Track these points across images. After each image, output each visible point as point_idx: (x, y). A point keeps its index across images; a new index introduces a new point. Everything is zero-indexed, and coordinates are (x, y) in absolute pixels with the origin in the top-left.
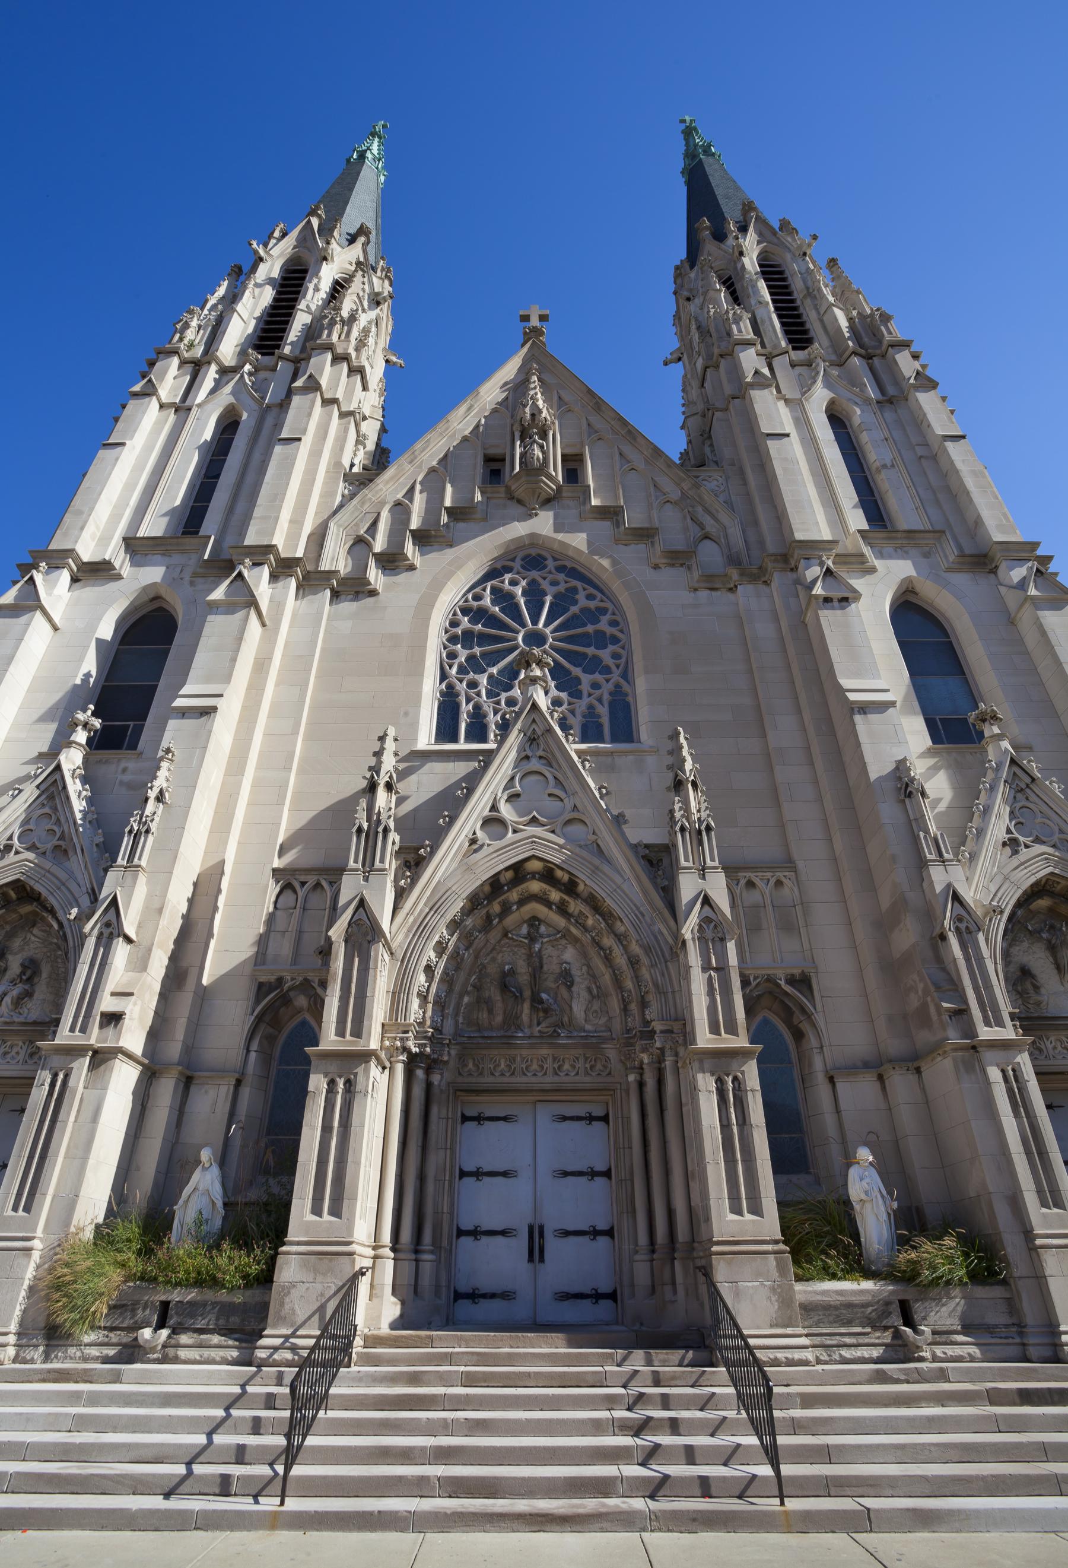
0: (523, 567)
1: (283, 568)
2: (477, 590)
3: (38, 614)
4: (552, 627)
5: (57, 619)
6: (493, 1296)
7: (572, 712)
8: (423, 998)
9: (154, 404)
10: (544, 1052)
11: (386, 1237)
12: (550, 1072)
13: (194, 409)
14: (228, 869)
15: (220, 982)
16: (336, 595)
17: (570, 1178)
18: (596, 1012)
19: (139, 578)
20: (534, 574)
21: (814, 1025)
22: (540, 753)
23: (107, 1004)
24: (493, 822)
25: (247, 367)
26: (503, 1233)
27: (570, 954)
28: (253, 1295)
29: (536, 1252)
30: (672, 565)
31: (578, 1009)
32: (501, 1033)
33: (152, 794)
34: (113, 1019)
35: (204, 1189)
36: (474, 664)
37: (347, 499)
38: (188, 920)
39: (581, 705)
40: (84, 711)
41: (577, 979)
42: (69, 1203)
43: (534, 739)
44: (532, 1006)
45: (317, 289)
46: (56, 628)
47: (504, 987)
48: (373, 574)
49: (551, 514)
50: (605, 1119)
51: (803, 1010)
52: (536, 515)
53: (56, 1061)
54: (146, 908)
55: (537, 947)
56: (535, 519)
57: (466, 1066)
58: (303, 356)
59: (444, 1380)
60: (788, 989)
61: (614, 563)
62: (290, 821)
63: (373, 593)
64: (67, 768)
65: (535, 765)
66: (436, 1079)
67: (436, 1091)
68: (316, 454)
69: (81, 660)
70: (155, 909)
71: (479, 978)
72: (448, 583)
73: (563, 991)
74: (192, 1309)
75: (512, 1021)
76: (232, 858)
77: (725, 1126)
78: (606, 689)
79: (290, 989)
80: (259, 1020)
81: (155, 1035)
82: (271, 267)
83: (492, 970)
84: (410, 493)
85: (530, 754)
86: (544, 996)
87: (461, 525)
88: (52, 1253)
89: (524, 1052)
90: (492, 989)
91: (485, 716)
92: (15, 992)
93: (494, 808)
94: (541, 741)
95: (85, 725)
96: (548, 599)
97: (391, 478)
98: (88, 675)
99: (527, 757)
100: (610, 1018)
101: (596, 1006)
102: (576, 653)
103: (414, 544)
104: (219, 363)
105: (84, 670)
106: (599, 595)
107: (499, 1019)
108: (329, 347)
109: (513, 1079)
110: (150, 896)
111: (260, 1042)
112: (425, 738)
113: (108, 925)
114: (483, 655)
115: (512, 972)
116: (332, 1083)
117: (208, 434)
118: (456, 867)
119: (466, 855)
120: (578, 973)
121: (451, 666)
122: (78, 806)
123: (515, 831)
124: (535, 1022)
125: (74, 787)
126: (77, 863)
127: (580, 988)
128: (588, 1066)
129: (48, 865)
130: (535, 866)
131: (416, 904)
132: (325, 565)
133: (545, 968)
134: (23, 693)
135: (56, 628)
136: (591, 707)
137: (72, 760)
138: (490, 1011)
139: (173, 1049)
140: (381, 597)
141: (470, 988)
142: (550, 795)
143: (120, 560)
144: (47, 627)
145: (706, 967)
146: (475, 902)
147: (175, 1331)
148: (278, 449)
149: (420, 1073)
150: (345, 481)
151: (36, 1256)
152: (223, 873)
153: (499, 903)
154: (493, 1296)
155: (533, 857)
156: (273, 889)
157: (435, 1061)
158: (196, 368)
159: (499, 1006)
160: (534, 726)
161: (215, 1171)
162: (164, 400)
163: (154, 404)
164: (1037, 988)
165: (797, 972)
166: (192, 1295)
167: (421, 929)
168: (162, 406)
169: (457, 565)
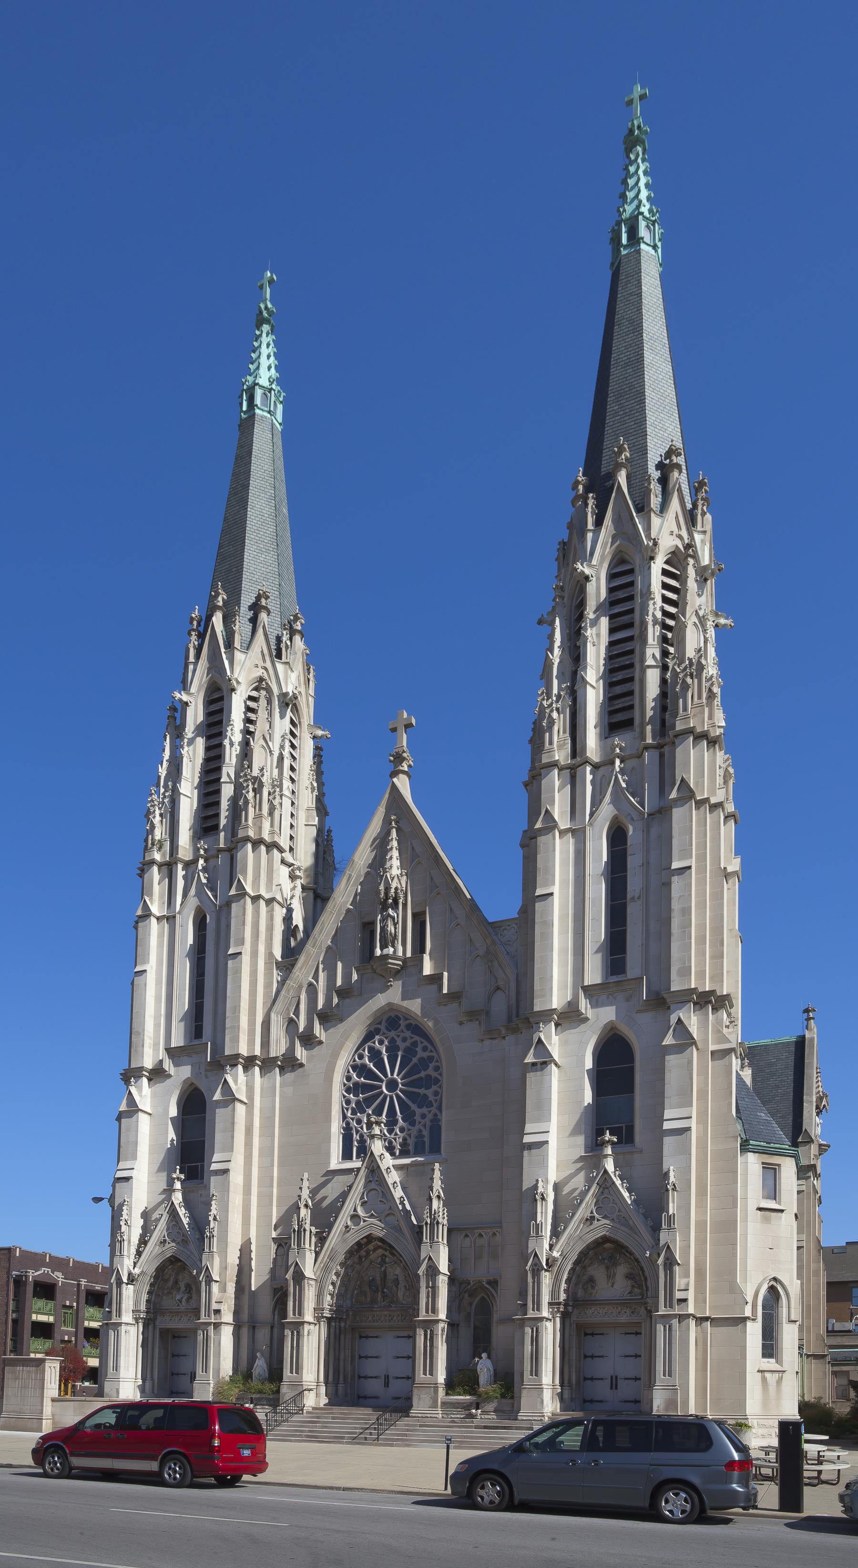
0: (387, 1029)
1: (249, 1062)
2: (360, 1051)
3: (140, 1114)
4: (401, 1075)
5: (149, 1111)
7: (410, 1135)
8: (332, 1295)
9: (154, 921)
10: (386, 1313)
11: (322, 1378)
13: (177, 916)
14: (253, 1241)
15: (259, 1289)
16: (282, 1069)
19: (180, 1074)
20: (393, 1034)
22: (376, 1179)
23: (214, 1306)
24: (355, 1217)
25: (201, 862)
26: (375, 1377)
27: (398, 1271)
28: (275, 1396)
30: (471, 1020)
31: (400, 1295)
33: (211, 1218)
34: (217, 1312)
35: (260, 1366)
36: (360, 1108)
37: (282, 983)
38: (240, 1267)
39: (414, 1131)
40: (175, 1172)
42: (217, 1370)
45: (232, 744)
46: (150, 1114)
48: (300, 1053)
49: (400, 982)
52: (391, 985)
53: (203, 1327)
54: (221, 1267)
56: (391, 989)
58: (233, 846)
59: (326, 1418)
61: (436, 1022)
62: (278, 1212)
63: (301, 1065)
64: (176, 1203)
65: (373, 1185)
68: (254, 954)
69: (167, 1133)
70: (224, 1268)
72: (340, 1052)
73: (394, 1287)
74: (259, 1399)
75: (374, 1301)
76: (255, 1234)
77: (425, 1347)
78: (430, 1116)
81: (236, 1313)
82: (195, 715)
84: (316, 977)
87: (347, 1001)
88: (215, 1385)
91: (366, 1141)
92: (185, 1298)
93: (355, 1210)
95: (178, 1179)
96: (400, 1054)
97: (303, 965)
98: (172, 1140)
99: (370, 1181)
102: (414, 1093)
103: (320, 1024)
104: (182, 861)
105: (170, 1139)
106: (430, 1047)
107: (369, 1299)
108: (247, 839)
110: (221, 1262)
112: (335, 1162)
113: (207, 1277)
114: (365, 1099)
115: (374, 1280)
116: (292, 1332)
117: (190, 940)
118: (339, 1239)
119: (344, 1234)
120: (401, 1279)
121: (347, 1109)
122: (185, 1221)
123: (364, 1221)
125: (182, 1212)
126: (192, 1246)
127: (401, 1286)
129: (182, 1248)
131: (323, 1258)
132: (273, 1054)
134: (147, 1156)
135: (150, 1114)
136: (420, 1131)
137: (178, 1198)
138: (366, 1297)
139: (245, 1317)
140: (306, 1067)
143: (168, 1065)
144: (146, 1116)
145: (427, 1287)
146: (350, 1253)
147: (256, 1405)
148: (230, 963)
149: (333, 1324)
150: (277, 968)
151: (212, 1385)
152: (251, 1243)
156: (274, 1247)
158: (168, 868)
161: (263, 1359)
162: (158, 914)
163: (154, 921)
164: (593, 1287)
165: (491, 1278)
166: (258, 1396)
167: (326, 1269)
168: (158, 919)
169: (346, 1036)
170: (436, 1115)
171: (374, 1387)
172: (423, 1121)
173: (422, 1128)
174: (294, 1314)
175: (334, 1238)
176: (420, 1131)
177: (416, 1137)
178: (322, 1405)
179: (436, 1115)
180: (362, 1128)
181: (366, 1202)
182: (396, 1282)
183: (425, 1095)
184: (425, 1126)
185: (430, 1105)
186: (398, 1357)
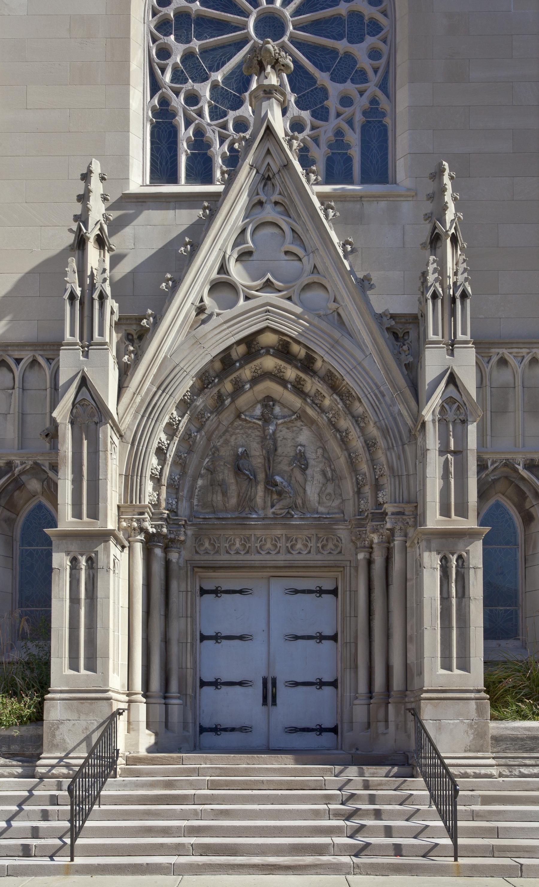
6: (233, 730)
8: (157, 480)
10: (278, 532)
12: (283, 550)
17: (300, 642)
18: (329, 494)
22: (276, 197)
24: (222, 286)
26: (241, 684)
27: (305, 436)
28: (29, 730)
29: (269, 695)
31: (312, 492)
32: (236, 515)
36: (193, 68)
41: (312, 462)
43: (269, 178)
44: (265, 487)
47: (238, 470)
50: (334, 592)
55: (271, 428)
57: (202, 545)
60: (525, 474)
66: (174, 556)
67: (174, 567)
71: (213, 461)
73: (297, 473)
75: (246, 503)
78: (361, 103)
79: (23, 472)
83: (225, 452)
85: (264, 198)
86: (278, 479)
89: (258, 533)
90: (226, 472)
93: (223, 269)
94: (277, 181)
99: (260, 203)
100: (343, 501)
101: (330, 489)
107: (233, 501)
109: (248, 557)
112: (138, 178)
114: (204, 51)
115: (246, 455)
116: (74, 561)
119: (194, 326)
127: (315, 470)
128: (320, 545)
130: (269, 339)
131: (142, 382)
133: (280, 450)
136: (339, 133)
138: (225, 494)
145: (444, 451)
149: (158, 552)
153: (231, 381)
154: (233, 730)
155: (267, 329)
157: (172, 541)
159: (233, 489)
160: (269, 160)
167: (149, 410)
170: (374, 101)
171: (239, 706)
172: (348, 111)
173: (345, 127)
174: (77, 514)
175: (170, 335)
176: (339, 133)
177: (330, 147)
178: (142, 752)
179: (374, 101)
180: (200, 114)
181: (249, 253)
183: (348, 56)
184: (350, 122)
185: (361, 77)
186: (296, 638)
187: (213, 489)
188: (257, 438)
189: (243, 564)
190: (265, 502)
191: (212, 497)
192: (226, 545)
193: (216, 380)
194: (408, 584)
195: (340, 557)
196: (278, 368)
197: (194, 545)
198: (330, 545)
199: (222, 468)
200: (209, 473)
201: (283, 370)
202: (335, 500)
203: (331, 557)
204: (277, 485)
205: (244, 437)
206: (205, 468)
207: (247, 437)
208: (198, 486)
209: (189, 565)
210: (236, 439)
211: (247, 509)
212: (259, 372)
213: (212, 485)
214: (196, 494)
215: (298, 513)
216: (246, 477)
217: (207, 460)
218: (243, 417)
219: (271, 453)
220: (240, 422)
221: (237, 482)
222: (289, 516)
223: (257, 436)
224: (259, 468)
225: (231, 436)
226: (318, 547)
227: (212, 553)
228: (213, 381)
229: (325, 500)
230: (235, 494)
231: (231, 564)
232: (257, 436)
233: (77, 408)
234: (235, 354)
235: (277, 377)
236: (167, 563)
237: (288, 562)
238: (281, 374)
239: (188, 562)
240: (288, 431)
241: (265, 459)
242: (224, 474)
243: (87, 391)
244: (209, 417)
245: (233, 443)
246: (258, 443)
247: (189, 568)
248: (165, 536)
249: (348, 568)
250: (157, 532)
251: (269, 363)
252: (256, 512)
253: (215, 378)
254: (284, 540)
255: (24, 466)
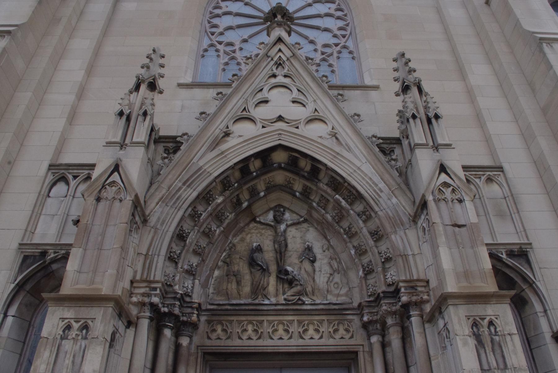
12: (296, 335)
18: (337, 283)
21: (536, 292)
31: (321, 280)
32: (249, 301)
41: (319, 256)
43: (280, 64)
44: (277, 277)
47: (252, 263)
51: (525, 279)
55: (283, 227)
57: (214, 330)
66: (184, 341)
67: (184, 352)
71: (229, 256)
73: (307, 265)
75: (258, 290)
80: (20, 287)
86: (289, 269)
89: (271, 318)
90: (241, 264)
101: (337, 278)
107: (247, 289)
109: (260, 342)
111: (19, 308)
115: (259, 249)
124: (281, 292)
127: (322, 263)
130: (280, 157)
133: (290, 246)
138: (238, 283)
141: (220, 263)
142: (294, 102)
149: (168, 333)
153: (248, 189)
155: (280, 146)
157: (185, 323)
159: (247, 278)
160: (280, 54)
182: (308, 255)
187: (228, 279)
188: (269, 237)
189: (254, 349)
190: (277, 290)
191: (227, 286)
192: (238, 330)
193: (236, 185)
194: (433, 363)
195: (352, 342)
196: (288, 180)
197: (207, 330)
198: (342, 331)
199: (238, 260)
200: (226, 265)
201: (292, 182)
202: (343, 289)
203: (343, 342)
204: (289, 274)
205: (259, 235)
206: (222, 261)
207: (261, 236)
208: (214, 276)
209: (199, 351)
210: (251, 237)
211: (260, 297)
212: (272, 183)
213: (227, 276)
214: (212, 283)
215: (309, 299)
216: (259, 268)
217: (224, 254)
218: (258, 219)
219: (281, 251)
220: (255, 225)
221: (251, 272)
222: (300, 302)
223: (270, 235)
224: (272, 261)
225: (247, 234)
226: (330, 332)
227: (224, 338)
228: (233, 185)
229: (333, 288)
230: (249, 284)
231: (243, 349)
232: (270, 235)
233: (106, 188)
234: (253, 167)
235: (287, 188)
236: (178, 347)
237: (300, 347)
238: (291, 185)
239: (199, 348)
240: (297, 231)
241: (277, 252)
242: (239, 265)
243: (118, 175)
244: (228, 216)
245: (248, 241)
246: (270, 240)
247: (200, 354)
248: (177, 317)
249: (362, 353)
250: (170, 311)
251: (279, 177)
252: (269, 299)
253: (235, 183)
254: (296, 326)
255: (56, 255)
